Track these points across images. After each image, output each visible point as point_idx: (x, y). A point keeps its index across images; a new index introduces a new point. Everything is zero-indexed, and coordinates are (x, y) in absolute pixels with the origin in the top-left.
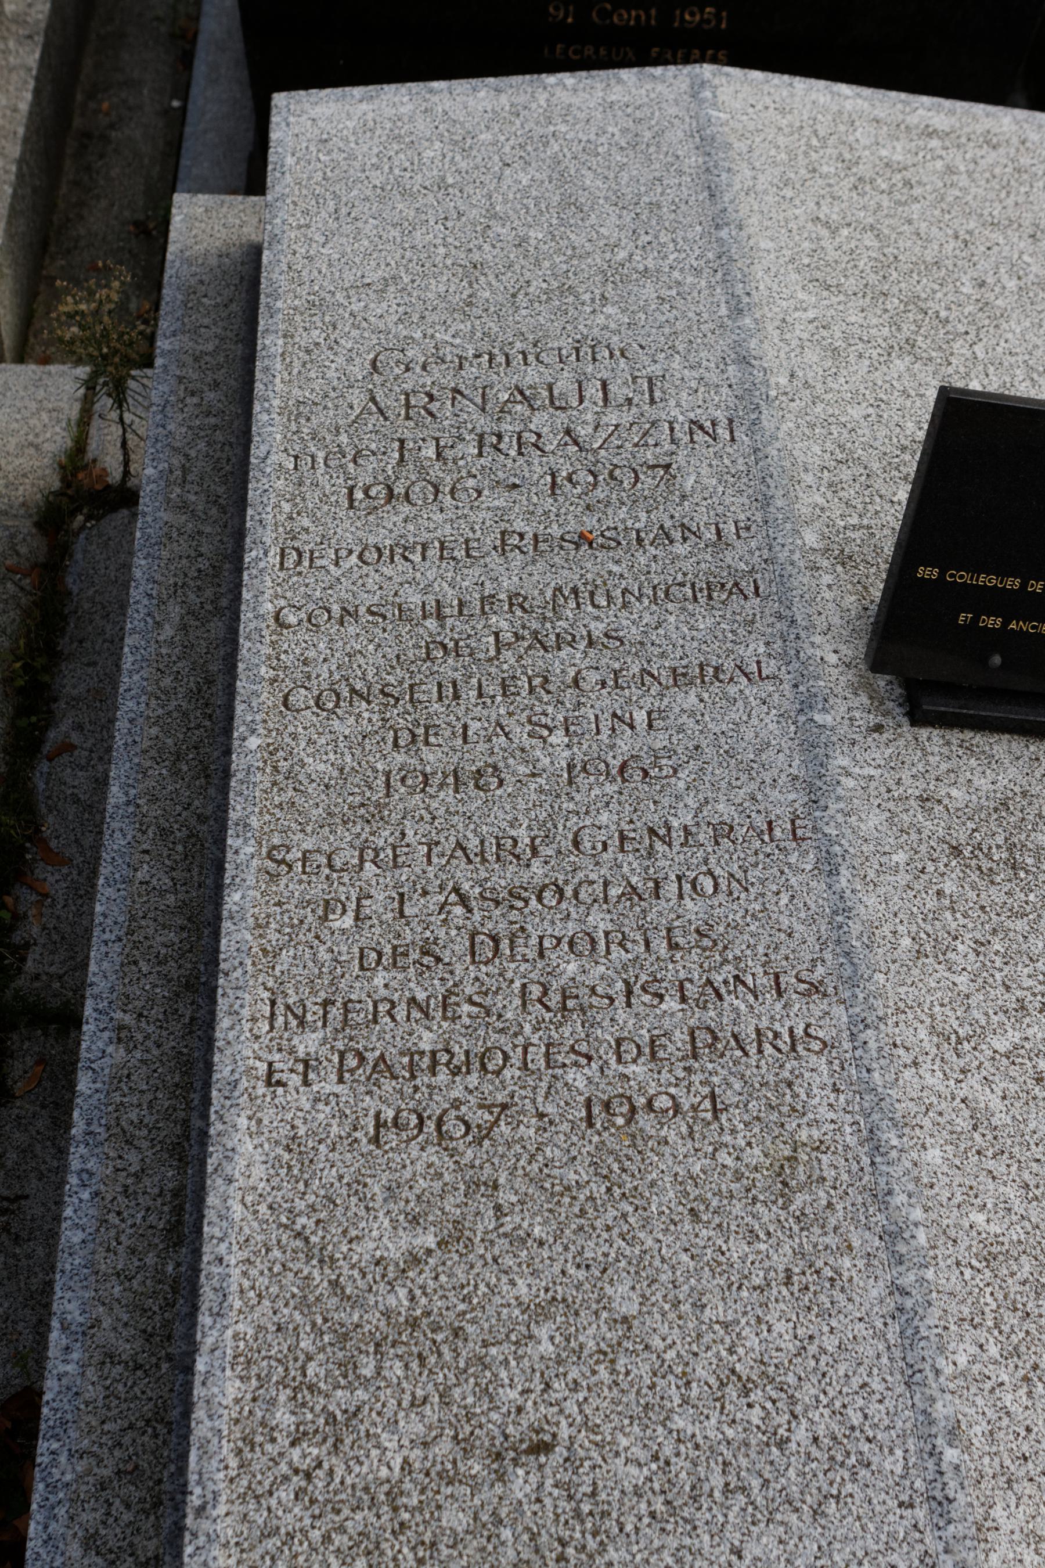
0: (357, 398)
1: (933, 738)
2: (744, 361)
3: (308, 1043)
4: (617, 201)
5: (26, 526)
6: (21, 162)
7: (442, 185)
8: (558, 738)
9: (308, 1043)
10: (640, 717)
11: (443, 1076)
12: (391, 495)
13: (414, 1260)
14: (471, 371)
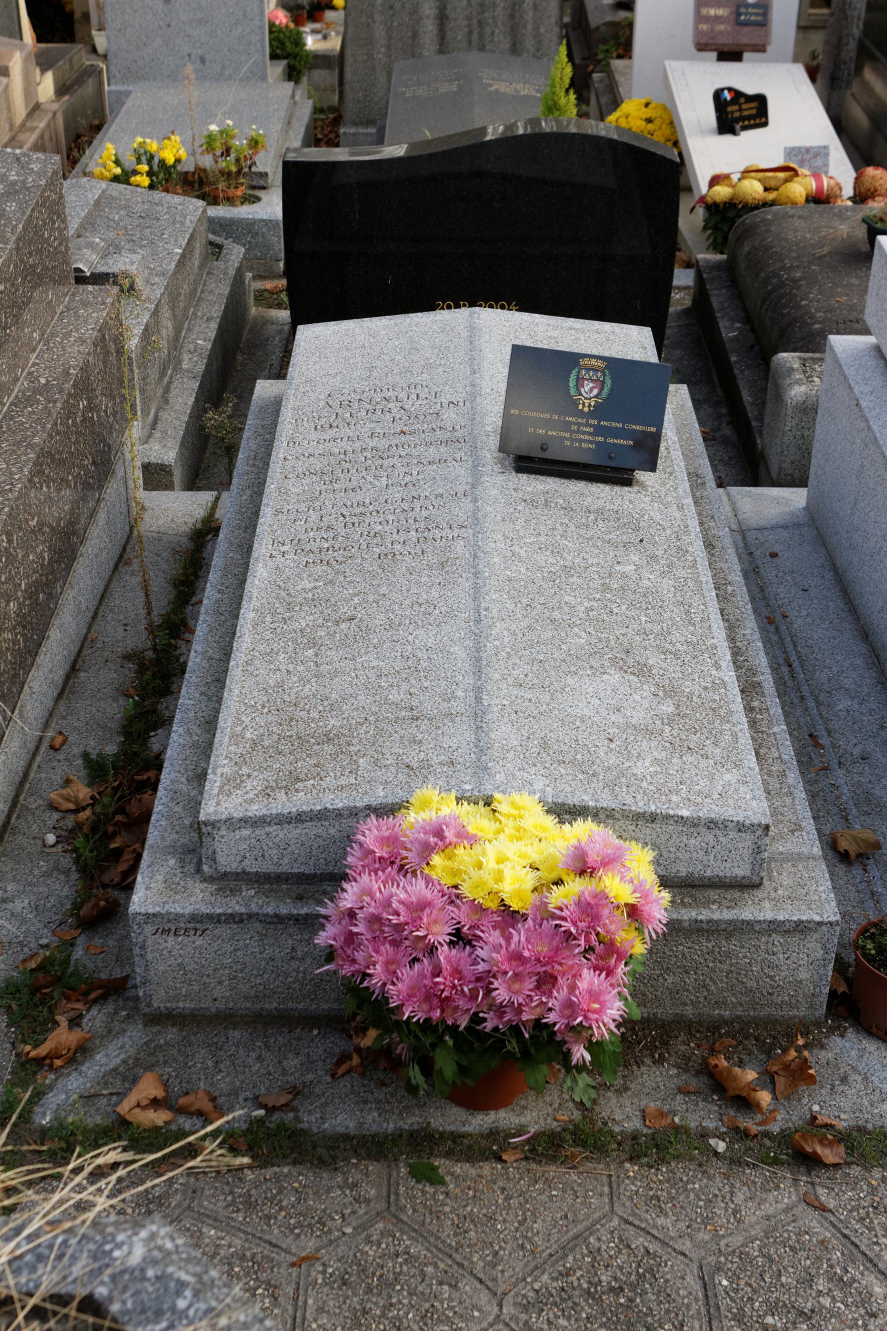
0: (322, 404)
1: (524, 477)
2: (473, 385)
4: (433, 347)
5: (185, 540)
6: (188, 423)
7: (364, 346)
11: (330, 552)
14: (365, 394)
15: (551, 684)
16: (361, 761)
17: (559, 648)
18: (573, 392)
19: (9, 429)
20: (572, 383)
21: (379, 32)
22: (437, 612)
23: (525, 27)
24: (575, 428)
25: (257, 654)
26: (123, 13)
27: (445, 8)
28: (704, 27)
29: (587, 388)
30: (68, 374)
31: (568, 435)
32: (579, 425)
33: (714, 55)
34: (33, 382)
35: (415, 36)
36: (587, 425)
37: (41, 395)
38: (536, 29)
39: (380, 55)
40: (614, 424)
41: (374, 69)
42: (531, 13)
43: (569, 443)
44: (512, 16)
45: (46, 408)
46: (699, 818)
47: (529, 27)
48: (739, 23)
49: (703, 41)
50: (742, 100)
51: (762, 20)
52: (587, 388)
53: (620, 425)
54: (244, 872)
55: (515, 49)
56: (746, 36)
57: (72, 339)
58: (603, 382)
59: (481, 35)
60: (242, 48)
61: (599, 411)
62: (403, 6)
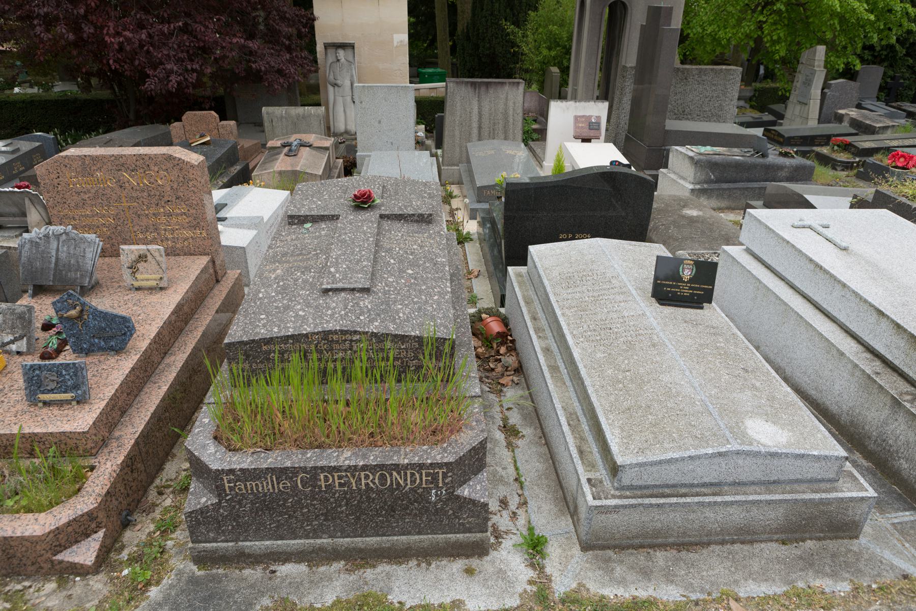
21: (457, 133)
35: (470, 134)
55: (506, 139)
56: (592, 133)
61: (691, 281)
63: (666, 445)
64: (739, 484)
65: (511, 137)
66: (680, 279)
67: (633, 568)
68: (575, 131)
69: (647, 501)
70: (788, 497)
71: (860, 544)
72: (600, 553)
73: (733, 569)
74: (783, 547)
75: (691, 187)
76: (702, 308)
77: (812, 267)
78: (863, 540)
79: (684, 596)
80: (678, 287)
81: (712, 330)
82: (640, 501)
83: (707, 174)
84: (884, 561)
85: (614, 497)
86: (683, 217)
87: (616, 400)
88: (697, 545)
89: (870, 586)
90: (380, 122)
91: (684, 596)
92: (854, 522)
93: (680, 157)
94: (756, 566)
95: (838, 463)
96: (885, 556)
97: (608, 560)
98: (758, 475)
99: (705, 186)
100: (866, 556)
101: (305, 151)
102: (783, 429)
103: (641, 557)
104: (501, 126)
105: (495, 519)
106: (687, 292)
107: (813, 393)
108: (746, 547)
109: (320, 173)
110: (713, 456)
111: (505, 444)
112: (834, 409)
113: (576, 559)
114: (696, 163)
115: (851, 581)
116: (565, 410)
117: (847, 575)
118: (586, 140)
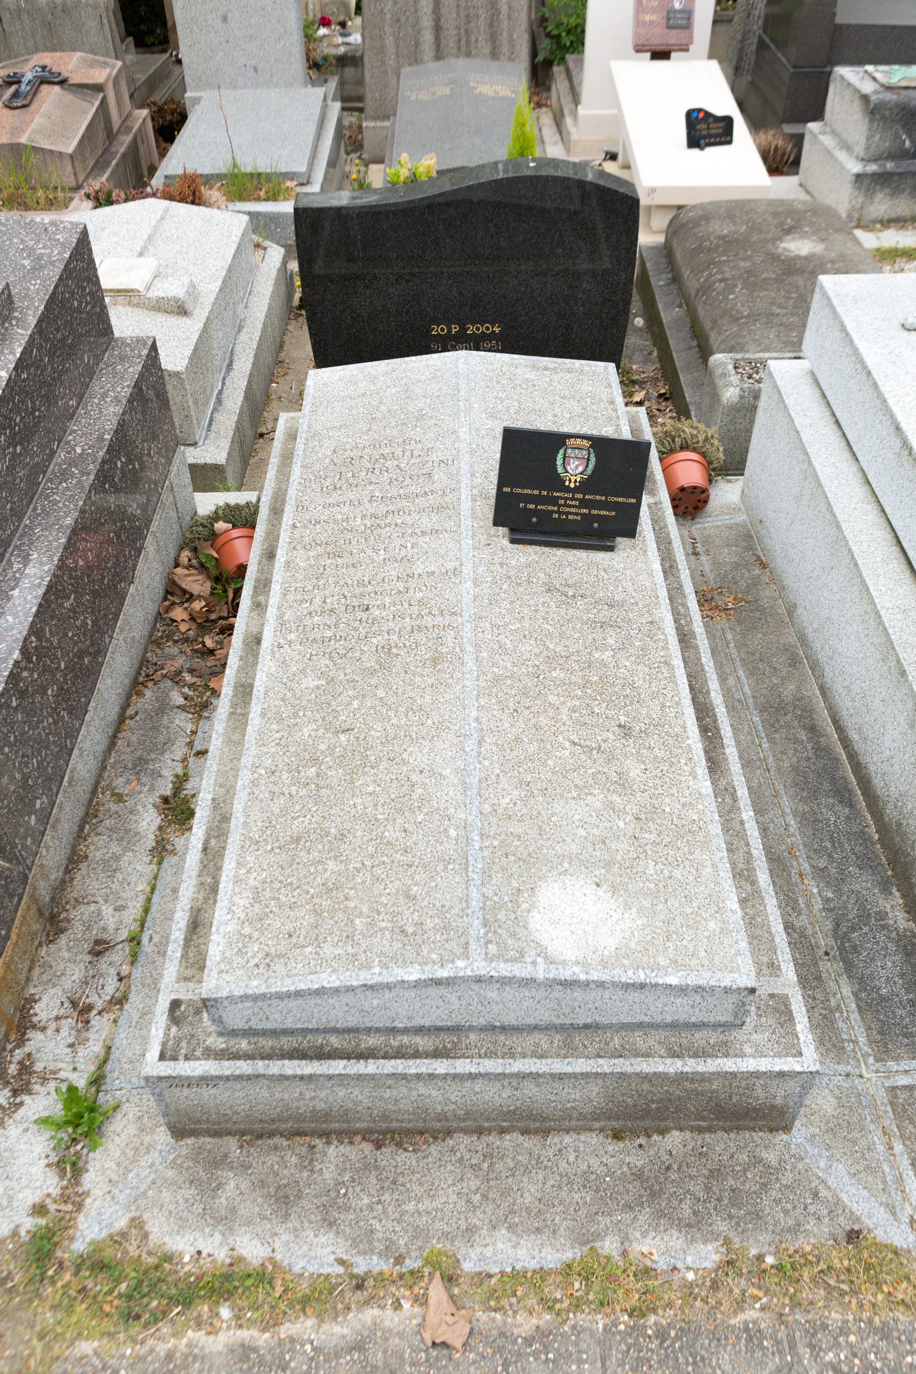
0: (327, 461)
3: (292, 636)
7: (364, 395)
8: (382, 552)
9: (292, 636)
10: (409, 545)
11: (332, 643)
12: (335, 488)
13: (318, 688)
14: (366, 451)
15: (539, 813)
16: (357, 921)
17: (545, 764)
18: (560, 470)
19: (43, 510)
20: (559, 462)
21: (389, 41)
22: (430, 722)
23: (501, 34)
24: (562, 502)
25: (263, 772)
26: (191, 32)
27: (439, 20)
28: (642, 31)
29: (573, 466)
30: (103, 440)
31: (556, 508)
32: (566, 499)
33: (648, 55)
34: (69, 453)
35: (417, 44)
36: (573, 499)
37: (76, 467)
38: (511, 35)
39: (391, 61)
40: (598, 498)
41: (386, 73)
42: (506, 22)
43: (556, 516)
44: (491, 25)
45: (80, 481)
46: (687, 985)
47: (505, 34)
48: (669, 27)
49: (641, 42)
50: (711, 120)
51: (681, 21)
52: (573, 466)
53: (603, 498)
54: (250, 1029)
55: (494, 55)
56: (673, 37)
57: (108, 400)
58: (588, 460)
59: (468, 42)
60: (285, 59)
61: (585, 486)
62: (407, 19)
63: (328, 950)
64: (503, 1029)
65: (505, 49)
66: (558, 483)
67: (263, 1184)
68: (636, 35)
69: (276, 1067)
70: (605, 1065)
71: (787, 1145)
72: (208, 1142)
73: (476, 1198)
74: (613, 1147)
75: (856, 167)
76: (611, 549)
77: (896, 443)
78: (799, 1135)
79: (341, 1262)
80: (554, 501)
81: (606, 613)
82: (260, 1066)
83: (897, 137)
84: (823, 1193)
85: (210, 1054)
86: (775, 258)
87: (284, 812)
88: (422, 1133)
89: (760, 1258)
90: (225, 19)
91: (341, 1262)
92: (773, 1107)
93: (847, 94)
94: (530, 1190)
95: (733, 998)
96: (831, 1181)
97: (218, 1162)
98: (545, 1016)
99: (890, 166)
100: (787, 1178)
101: (51, 93)
102: (627, 907)
103: (282, 1162)
104: (482, 22)
105: (36, 1040)
106: (574, 513)
107: (854, 736)
108: (528, 1143)
109: (70, 150)
110: (417, 984)
111: (151, 843)
112: (877, 782)
113: (155, 1156)
114: (874, 111)
115: (727, 1242)
116: (215, 808)
117: (722, 1226)
118: (661, 55)
